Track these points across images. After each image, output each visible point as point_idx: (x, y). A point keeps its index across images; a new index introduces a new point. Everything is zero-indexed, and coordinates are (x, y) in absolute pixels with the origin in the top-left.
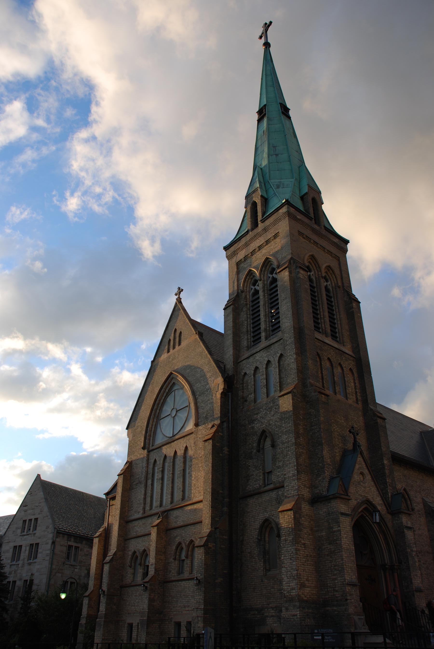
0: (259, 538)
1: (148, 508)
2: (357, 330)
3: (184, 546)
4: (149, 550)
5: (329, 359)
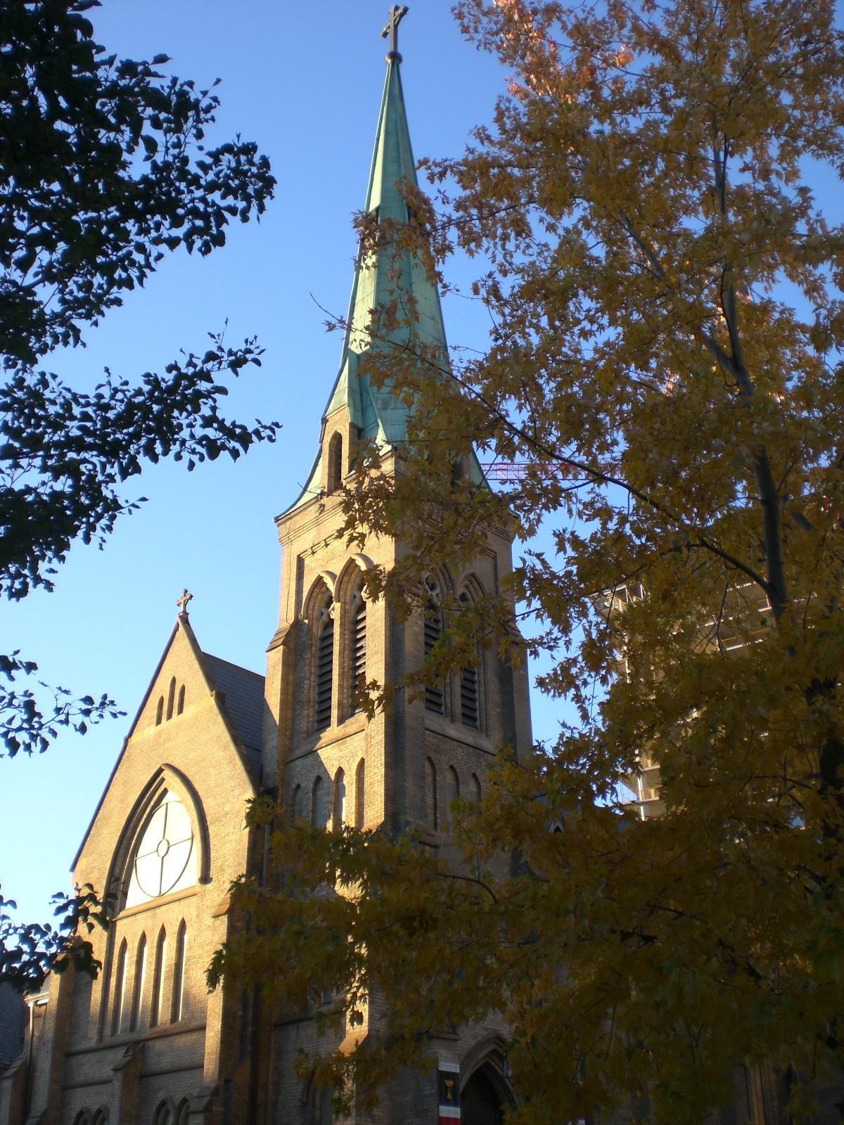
0: (304, 1100)
1: (108, 1031)
2: (516, 704)
3: (170, 1107)
4: (108, 1112)
5: (452, 767)
